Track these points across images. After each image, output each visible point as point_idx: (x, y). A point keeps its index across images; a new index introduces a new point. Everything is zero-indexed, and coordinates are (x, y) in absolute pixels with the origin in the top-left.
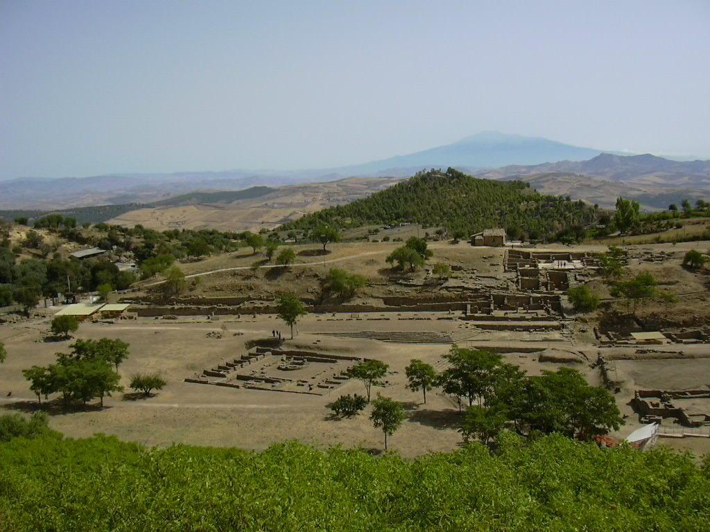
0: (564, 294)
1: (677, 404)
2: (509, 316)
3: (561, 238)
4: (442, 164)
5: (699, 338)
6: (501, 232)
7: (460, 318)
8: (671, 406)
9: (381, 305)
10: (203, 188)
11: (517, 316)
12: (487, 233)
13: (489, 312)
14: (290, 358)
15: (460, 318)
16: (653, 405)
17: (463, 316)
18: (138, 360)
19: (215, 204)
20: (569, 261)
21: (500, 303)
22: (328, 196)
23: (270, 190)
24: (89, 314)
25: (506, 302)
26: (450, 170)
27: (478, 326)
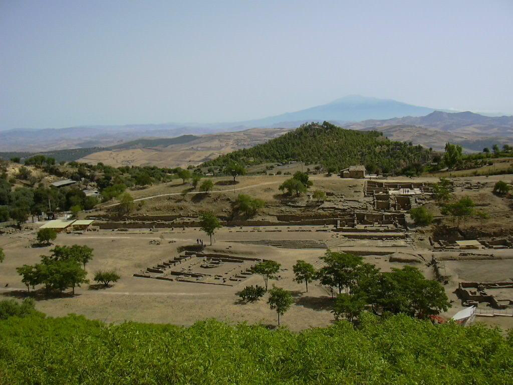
0: (407, 213)
1: (489, 292)
2: (368, 228)
3: (405, 172)
4: (320, 119)
5: (505, 244)
6: (362, 168)
7: (333, 230)
8: (485, 294)
9: (276, 220)
10: (147, 136)
11: (374, 228)
12: (352, 168)
13: (353, 226)
14: (209, 259)
15: (333, 230)
16: (472, 293)
17: (335, 228)
18: (100, 261)
19: (156, 148)
20: (411, 189)
21: (361, 219)
22: (237, 142)
23: (195, 138)
24: (64, 227)
25: (365, 218)
26: (325, 123)
27: (345, 236)
